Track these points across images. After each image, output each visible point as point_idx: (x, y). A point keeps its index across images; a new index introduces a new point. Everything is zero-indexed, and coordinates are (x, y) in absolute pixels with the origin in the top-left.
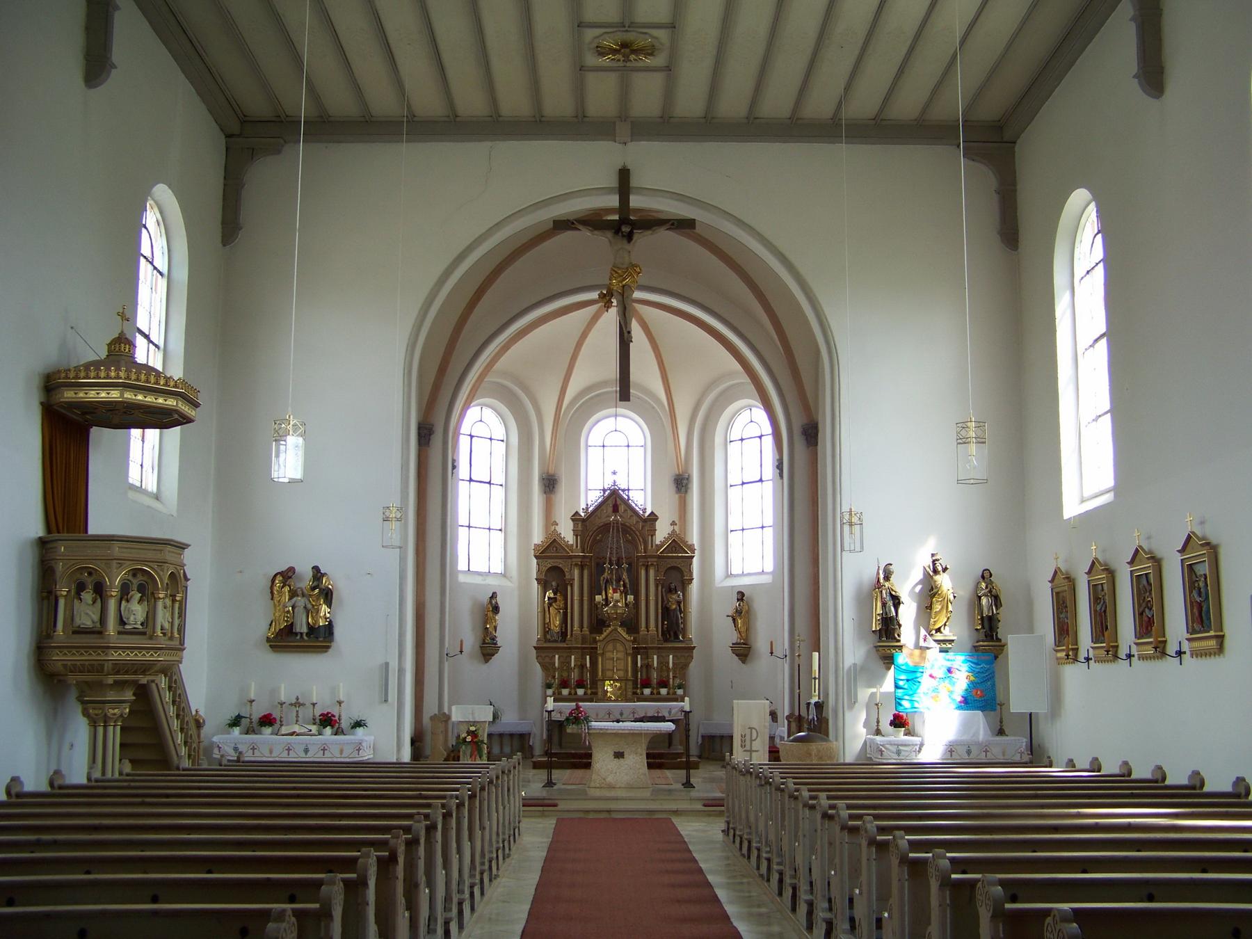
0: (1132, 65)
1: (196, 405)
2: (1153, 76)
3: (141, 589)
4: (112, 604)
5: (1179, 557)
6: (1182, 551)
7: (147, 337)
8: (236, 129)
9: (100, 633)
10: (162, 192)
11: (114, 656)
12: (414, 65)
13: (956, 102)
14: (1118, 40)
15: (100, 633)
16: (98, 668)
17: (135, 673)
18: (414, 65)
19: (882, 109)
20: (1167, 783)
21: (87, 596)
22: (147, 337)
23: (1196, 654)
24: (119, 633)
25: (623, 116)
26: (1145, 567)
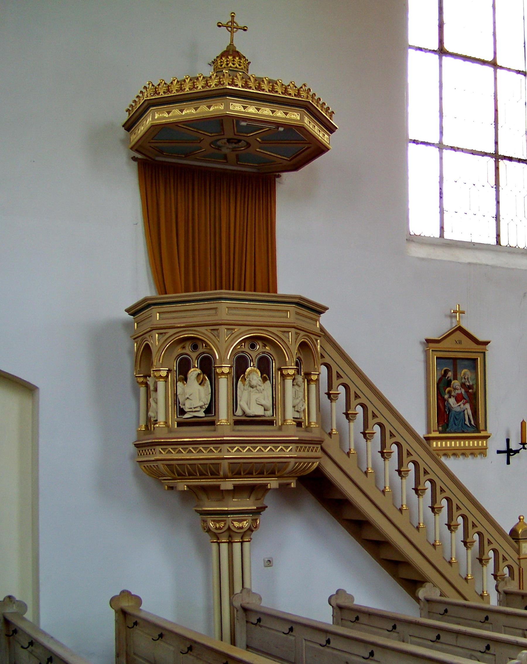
1: (331, 129)
3: (264, 366)
4: (223, 384)
9: (212, 423)
11: (232, 453)
15: (212, 423)
16: (212, 470)
17: (261, 474)
21: (253, 374)
24: (180, 424)
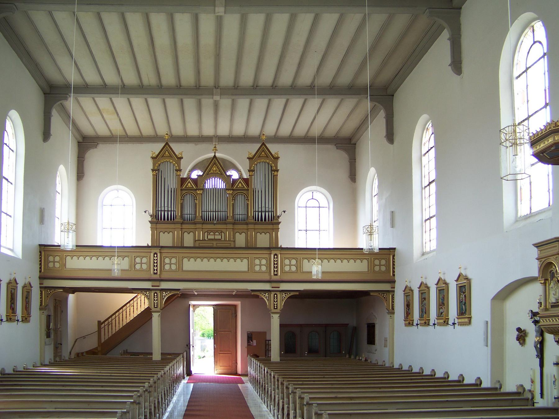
0: (449, 60)
2: (457, 65)
5: (456, 283)
6: (457, 281)
7: (7, 180)
8: (81, 140)
10: (14, 114)
12: (124, 61)
13: (367, 78)
14: (442, 47)
18: (124, 61)
19: (334, 78)
20: (436, 376)
22: (7, 180)
23: (461, 324)
25: (217, 86)
26: (462, 282)
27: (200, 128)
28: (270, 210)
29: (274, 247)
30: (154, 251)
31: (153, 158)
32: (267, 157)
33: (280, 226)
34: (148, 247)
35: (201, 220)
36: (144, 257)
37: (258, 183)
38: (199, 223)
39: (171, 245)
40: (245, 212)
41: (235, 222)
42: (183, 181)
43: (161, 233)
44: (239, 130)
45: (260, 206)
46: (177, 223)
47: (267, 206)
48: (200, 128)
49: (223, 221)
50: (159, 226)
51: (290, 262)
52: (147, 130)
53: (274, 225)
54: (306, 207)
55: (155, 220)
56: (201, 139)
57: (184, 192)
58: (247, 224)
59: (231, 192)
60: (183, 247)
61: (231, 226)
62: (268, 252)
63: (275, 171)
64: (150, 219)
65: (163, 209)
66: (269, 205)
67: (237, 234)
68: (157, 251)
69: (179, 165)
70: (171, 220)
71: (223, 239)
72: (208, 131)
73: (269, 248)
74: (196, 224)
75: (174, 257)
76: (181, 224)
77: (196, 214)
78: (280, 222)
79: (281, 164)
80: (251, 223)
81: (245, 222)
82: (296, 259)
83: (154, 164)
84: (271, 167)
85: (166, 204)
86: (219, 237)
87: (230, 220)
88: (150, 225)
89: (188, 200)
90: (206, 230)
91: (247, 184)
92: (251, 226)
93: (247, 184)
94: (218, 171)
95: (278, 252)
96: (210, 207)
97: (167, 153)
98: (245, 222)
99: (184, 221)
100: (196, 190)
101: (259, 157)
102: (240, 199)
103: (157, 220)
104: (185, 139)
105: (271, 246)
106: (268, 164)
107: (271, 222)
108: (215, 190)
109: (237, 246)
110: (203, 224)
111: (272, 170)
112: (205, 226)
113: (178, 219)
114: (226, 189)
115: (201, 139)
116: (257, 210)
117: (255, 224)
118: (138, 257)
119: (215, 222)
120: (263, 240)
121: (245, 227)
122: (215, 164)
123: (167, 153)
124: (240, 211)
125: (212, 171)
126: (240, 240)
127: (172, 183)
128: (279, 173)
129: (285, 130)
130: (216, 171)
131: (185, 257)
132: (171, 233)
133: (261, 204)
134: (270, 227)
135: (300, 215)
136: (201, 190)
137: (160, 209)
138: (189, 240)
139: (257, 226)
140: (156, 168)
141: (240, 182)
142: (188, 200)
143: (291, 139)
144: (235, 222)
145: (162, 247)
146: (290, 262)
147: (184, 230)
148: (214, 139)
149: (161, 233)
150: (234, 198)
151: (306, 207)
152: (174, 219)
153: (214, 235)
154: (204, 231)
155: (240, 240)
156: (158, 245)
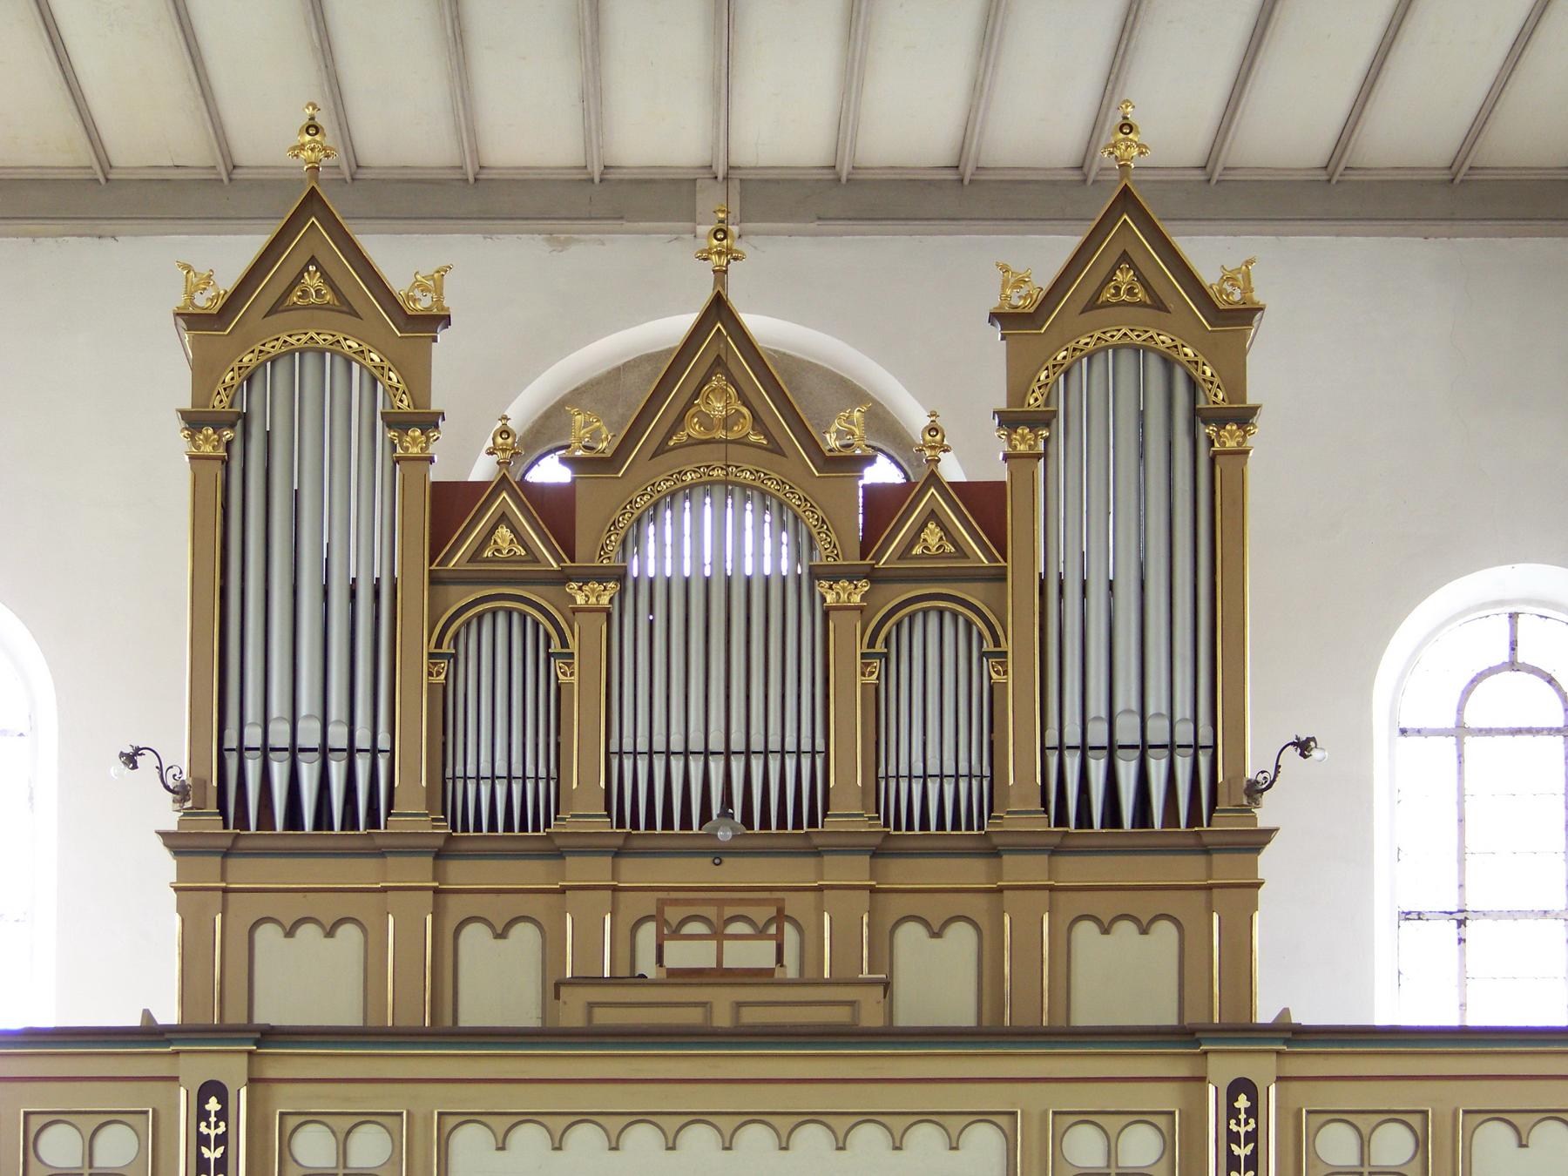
27: (593, 96)
28: (1184, 734)
29: (1211, 1027)
30: (199, 1066)
31: (193, 320)
32: (1158, 305)
33: (1268, 862)
34: (149, 1034)
35: (604, 826)
36: (113, 1117)
37: (1097, 526)
38: (587, 847)
39: (351, 1017)
40: (972, 759)
41: (895, 836)
42: (452, 505)
43: (268, 935)
44: (912, 120)
45: (1097, 707)
46: (407, 848)
47: (1157, 702)
48: (593, 96)
49: (794, 825)
50: (244, 873)
51: (1364, 1144)
52: (147, 124)
53: (1218, 859)
54: (1460, 731)
55: (213, 824)
56: (600, 197)
57: (461, 596)
58: (995, 853)
59: (853, 593)
60: (447, 1034)
61: (855, 870)
62: (1182, 1068)
63: (1221, 418)
64: (171, 821)
65: (280, 735)
66: (1172, 705)
67: (910, 937)
68: (230, 1067)
69: (418, 377)
70: (350, 822)
71: (791, 971)
72: (658, 125)
73: (1184, 1036)
74: (559, 854)
75: (368, 1118)
76: (440, 855)
77: (558, 778)
78: (1268, 834)
79: (1269, 369)
80: (1026, 846)
81: (974, 832)
82: (1417, 1121)
83: (204, 372)
84: (1193, 385)
85: (307, 704)
86: (759, 954)
87: (849, 813)
88: (167, 866)
89: (495, 668)
90: (648, 904)
91: (996, 535)
92: (1021, 869)
93: (996, 535)
94: (744, 428)
95: (1260, 1067)
96: (688, 720)
97: (312, 281)
98: (974, 832)
99: (458, 832)
100: (562, 578)
101: (1093, 305)
102: (935, 658)
103: (234, 823)
104: (474, 195)
105: (1194, 1018)
106: (1168, 363)
107: (1194, 828)
108: (724, 594)
109: (903, 1020)
110: (618, 853)
111: (1196, 416)
112: (635, 872)
113: (412, 814)
114: (816, 574)
115: (600, 197)
116: (1072, 736)
117: (1055, 851)
118: (57, 1117)
119: (725, 835)
120: (1121, 972)
121: (973, 872)
122: (719, 364)
123: (312, 281)
124: (932, 748)
125: (694, 429)
126: (937, 974)
127: (354, 530)
128: (1260, 440)
129: (1293, 121)
130: (727, 423)
131: (471, 1118)
132: (349, 933)
133: (1116, 693)
134: (1189, 869)
135: (1406, 788)
136: (602, 576)
137: (253, 737)
138: (500, 977)
139: (1074, 870)
140: (220, 402)
141: (933, 515)
142: (495, 668)
143: (1341, 194)
144: (895, 836)
145: (270, 1036)
146: (1364, 1144)
147: (457, 907)
148: (710, 200)
149: (268, 935)
150: (882, 650)
151: (1460, 731)
152: (373, 821)
153: (718, 935)
154: (627, 919)
155: (937, 974)
156: (236, 1017)
